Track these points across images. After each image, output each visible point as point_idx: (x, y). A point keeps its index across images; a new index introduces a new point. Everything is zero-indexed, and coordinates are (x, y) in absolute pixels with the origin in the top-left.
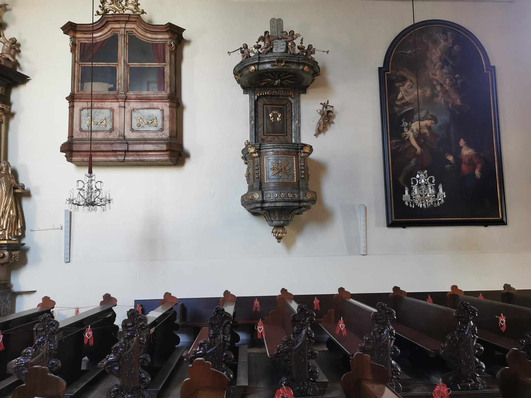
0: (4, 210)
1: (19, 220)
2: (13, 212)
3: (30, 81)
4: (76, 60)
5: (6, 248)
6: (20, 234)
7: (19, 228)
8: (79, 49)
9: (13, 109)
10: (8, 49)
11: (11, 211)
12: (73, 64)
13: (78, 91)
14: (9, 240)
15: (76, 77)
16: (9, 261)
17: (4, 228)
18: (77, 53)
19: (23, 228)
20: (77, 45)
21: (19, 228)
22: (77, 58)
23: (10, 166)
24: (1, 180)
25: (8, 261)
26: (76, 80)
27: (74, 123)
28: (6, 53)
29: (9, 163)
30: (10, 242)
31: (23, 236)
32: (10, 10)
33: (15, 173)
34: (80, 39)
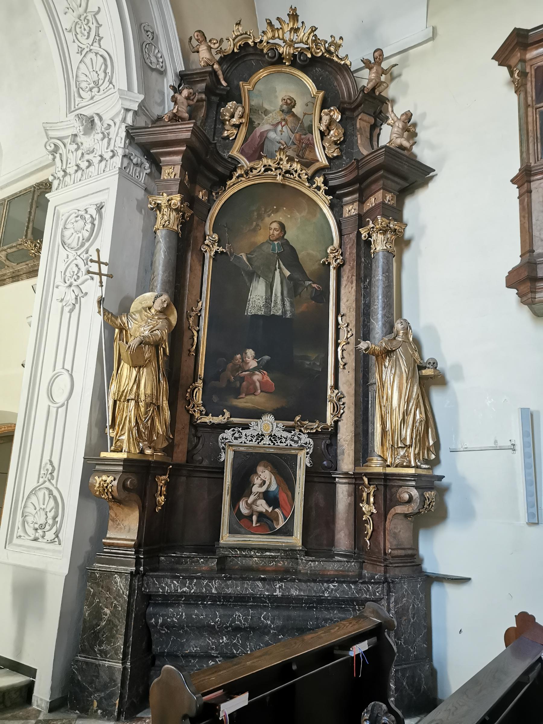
0: (405, 408)
1: (430, 430)
2: (421, 413)
3: (435, 178)
4: (530, 102)
5: (414, 483)
6: (433, 457)
7: (431, 444)
8: (534, 80)
9: (408, 233)
10: (400, 130)
11: (418, 412)
12: (523, 110)
13: (537, 160)
14: (417, 467)
15: (530, 134)
16: (421, 510)
17: (408, 443)
18: (529, 89)
19: (437, 445)
20: (529, 75)
21: (431, 444)
22: (529, 99)
23: (410, 328)
24: (398, 353)
25: (417, 511)
26: (531, 139)
27: (533, 223)
28: (397, 138)
29: (409, 324)
30: (420, 471)
31: (437, 462)
32: (400, 75)
33: (417, 342)
34: (534, 62)
